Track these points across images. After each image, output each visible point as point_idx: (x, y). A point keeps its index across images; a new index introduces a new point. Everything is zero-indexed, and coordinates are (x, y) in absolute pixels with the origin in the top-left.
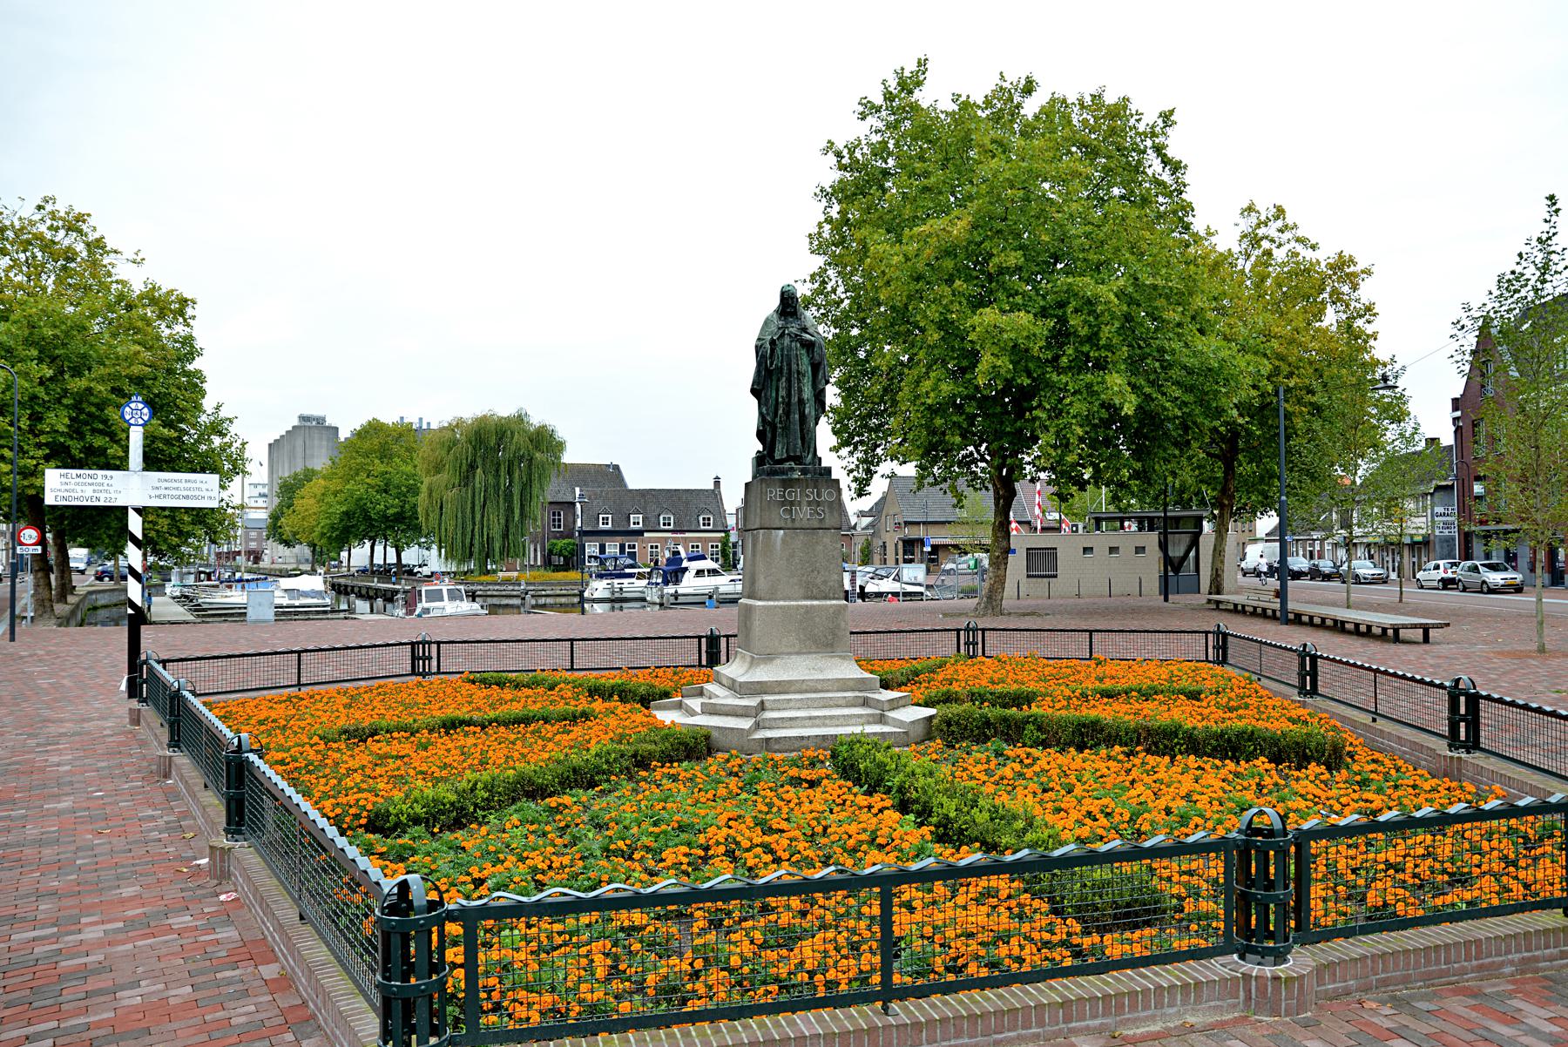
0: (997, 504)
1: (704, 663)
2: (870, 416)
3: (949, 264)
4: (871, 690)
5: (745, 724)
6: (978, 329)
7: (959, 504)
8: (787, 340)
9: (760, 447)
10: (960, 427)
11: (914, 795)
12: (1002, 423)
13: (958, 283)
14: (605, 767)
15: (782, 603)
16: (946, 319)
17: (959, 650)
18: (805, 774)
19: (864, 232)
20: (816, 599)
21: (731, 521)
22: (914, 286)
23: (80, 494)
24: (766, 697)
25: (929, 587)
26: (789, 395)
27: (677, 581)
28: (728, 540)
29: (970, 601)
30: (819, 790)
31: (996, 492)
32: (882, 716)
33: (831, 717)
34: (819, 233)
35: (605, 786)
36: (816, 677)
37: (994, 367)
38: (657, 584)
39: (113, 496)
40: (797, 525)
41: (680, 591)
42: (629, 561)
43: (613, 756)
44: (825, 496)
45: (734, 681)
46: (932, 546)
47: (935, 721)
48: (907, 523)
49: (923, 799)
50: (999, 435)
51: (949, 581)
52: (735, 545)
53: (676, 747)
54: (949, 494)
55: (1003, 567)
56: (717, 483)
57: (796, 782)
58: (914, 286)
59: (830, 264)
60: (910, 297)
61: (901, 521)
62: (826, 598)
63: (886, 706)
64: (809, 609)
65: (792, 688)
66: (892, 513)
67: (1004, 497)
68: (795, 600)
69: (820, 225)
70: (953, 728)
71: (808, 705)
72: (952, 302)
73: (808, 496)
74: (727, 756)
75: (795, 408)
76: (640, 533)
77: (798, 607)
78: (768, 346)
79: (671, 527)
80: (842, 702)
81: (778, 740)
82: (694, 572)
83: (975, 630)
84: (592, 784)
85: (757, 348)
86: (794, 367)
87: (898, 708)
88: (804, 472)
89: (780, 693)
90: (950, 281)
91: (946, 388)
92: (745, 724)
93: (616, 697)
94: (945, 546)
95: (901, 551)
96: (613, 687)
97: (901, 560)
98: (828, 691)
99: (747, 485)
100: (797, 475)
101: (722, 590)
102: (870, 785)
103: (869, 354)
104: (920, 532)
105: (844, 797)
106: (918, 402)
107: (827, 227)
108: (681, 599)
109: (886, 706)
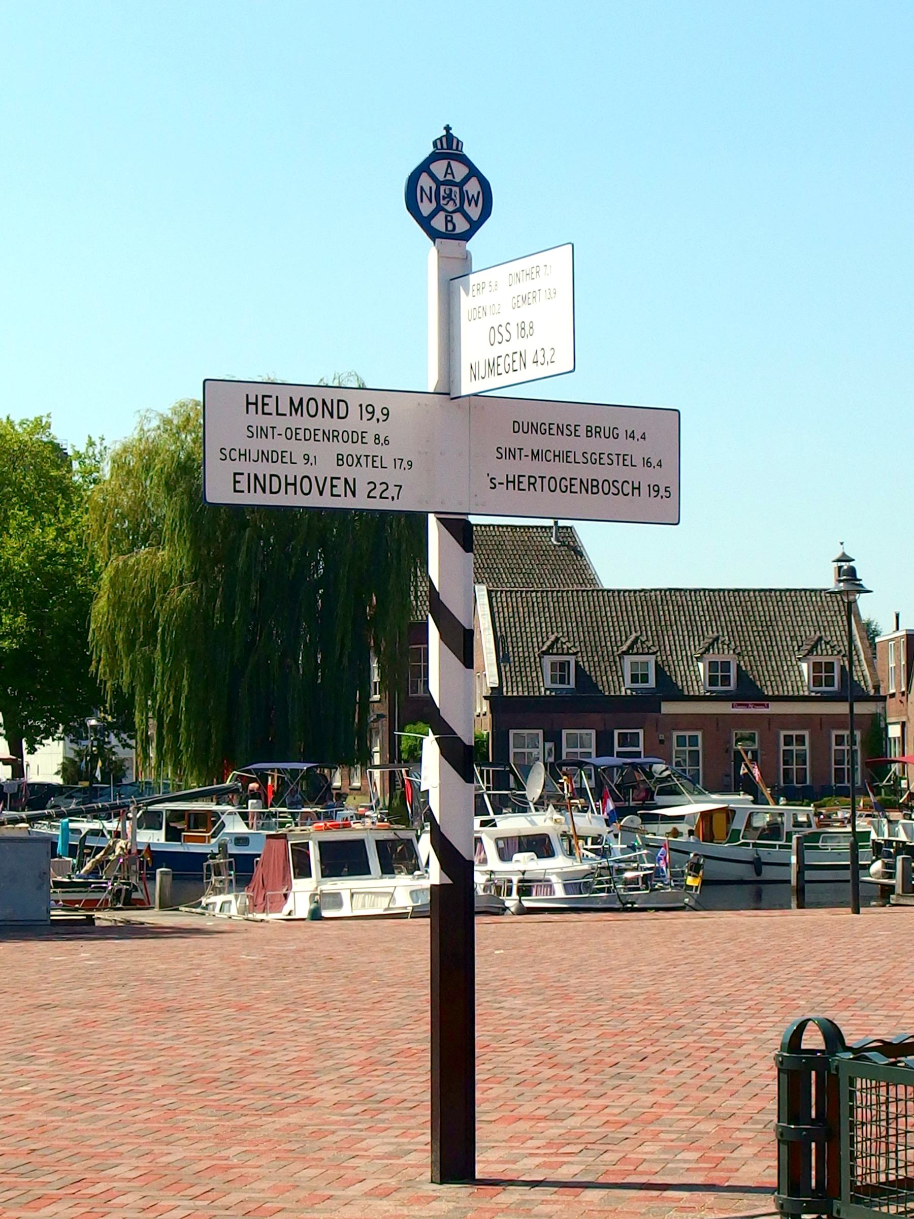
23: (300, 469)
39: (392, 476)
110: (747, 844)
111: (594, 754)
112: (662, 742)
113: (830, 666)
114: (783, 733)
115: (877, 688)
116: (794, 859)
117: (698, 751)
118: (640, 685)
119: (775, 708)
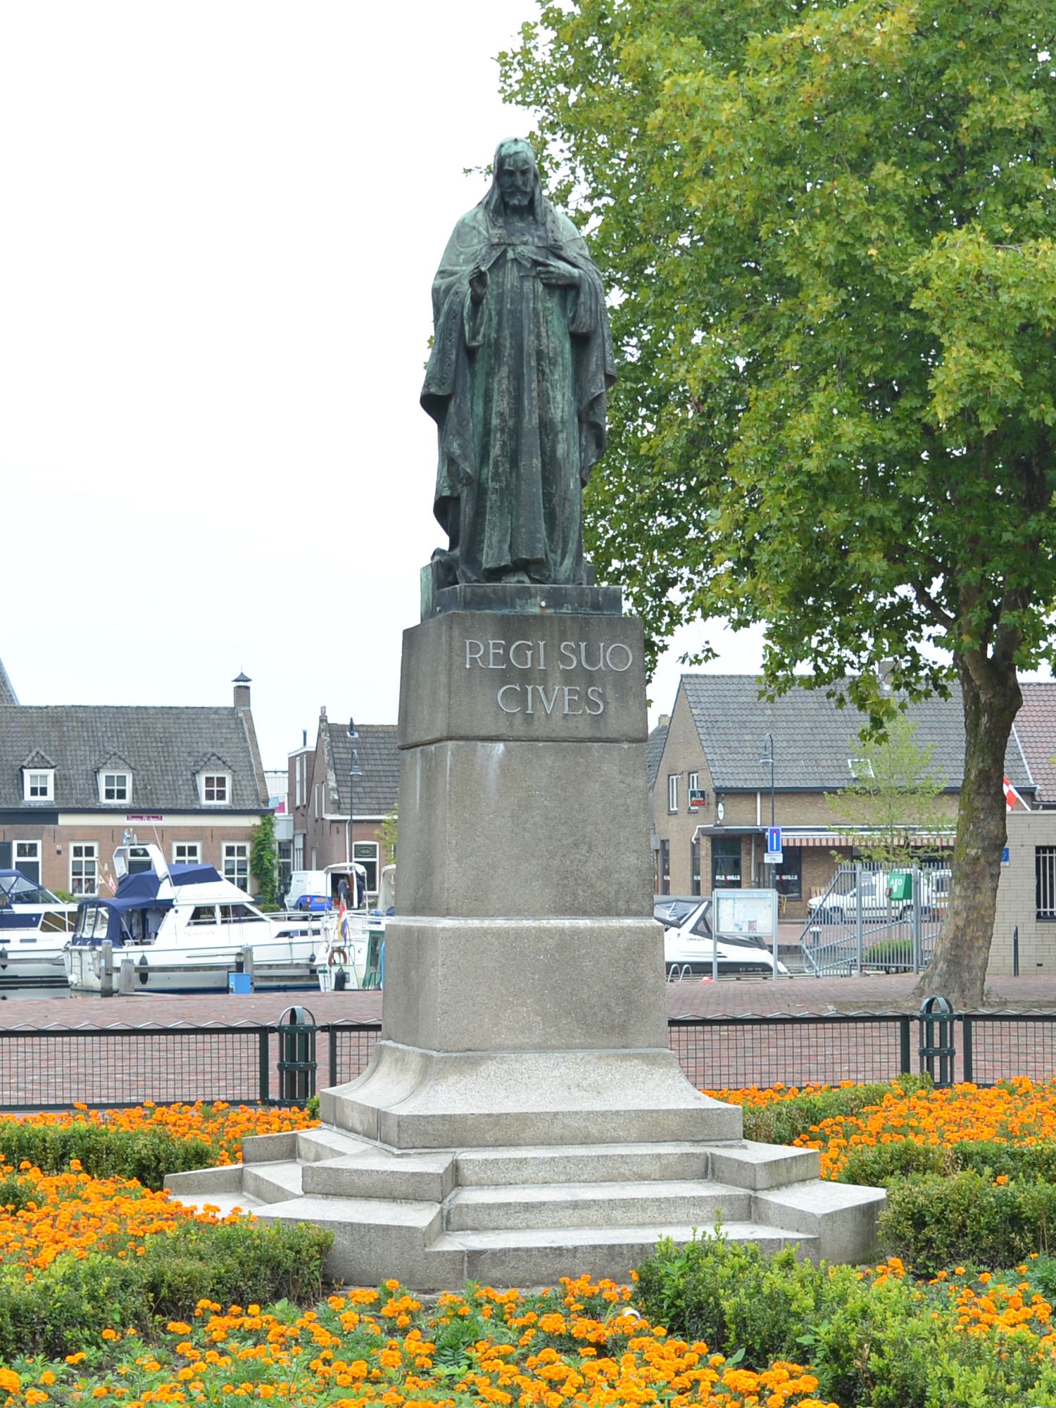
0: (972, 726)
1: (274, 1095)
2: (651, 507)
3: (859, 122)
4: (723, 1138)
5: (420, 1216)
6: (936, 283)
8: (511, 276)
9: (442, 540)
10: (884, 531)
11: (875, 1363)
12: (990, 521)
13: (882, 169)
14: (87, 1307)
15: (500, 923)
16: (853, 260)
17: (906, 1067)
18: (582, 1327)
19: (648, 42)
20: (585, 913)
21: (277, 789)
22: (773, 177)
24: (465, 1155)
25: (786, 952)
26: (517, 410)
27: (146, 935)
28: (268, 835)
29: (894, 979)
30: (629, 1357)
31: (972, 699)
32: (752, 1202)
33: (628, 1204)
34: (526, 52)
35: (86, 1354)
36: (586, 1107)
37: (976, 377)
38: (95, 942)
40: (539, 729)
41: (153, 960)
42: (25, 886)
43: (106, 1281)
45: (380, 1116)
46: (787, 851)
47: (885, 1215)
48: (723, 793)
49: (898, 1369)
50: (981, 550)
51: (830, 935)
52: (285, 849)
53: (251, 1267)
54: (851, 708)
55: (987, 884)
56: (242, 691)
57: (568, 1345)
58: (773, 177)
59: (552, 127)
60: (763, 205)
61: (708, 788)
62: (608, 911)
63: (762, 1179)
64: (566, 940)
65: (529, 1133)
66: (682, 766)
67: (991, 710)
68: (534, 915)
69: (527, 32)
70: (931, 1232)
71: (567, 1173)
72: (867, 217)
73: (565, 660)
74: (374, 1293)
75: (531, 442)
76: (47, 816)
77: (541, 933)
78: (466, 288)
79: (127, 801)
81: (500, 1256)
82: (191, 911)
83: (947, 1020)
84: (56, 1350)
85: (439, 296)
86: (529, 341)
87: (788, 1184)
88: (555, 599)
89: (497, 1144)
90: (861, 167)
91: (852, 431)
92: (420, 1216)
93: (75, 1164)
94: (821, 853)
95: (706, 864)
96: (65, 1141)
97: (706, 885)
98: (615, 1141)
99: (409, 635)
100: (537, 607)
101: (259, 956)
102: (749, 1351)
103: (649, 353)
104: (756, 816)
105: (695, 1374)
106: (781, 469)
107: (546, 35)
108: (155, 980)
109: (762, 1179)
112: (59, 852)
117: (37, 863)
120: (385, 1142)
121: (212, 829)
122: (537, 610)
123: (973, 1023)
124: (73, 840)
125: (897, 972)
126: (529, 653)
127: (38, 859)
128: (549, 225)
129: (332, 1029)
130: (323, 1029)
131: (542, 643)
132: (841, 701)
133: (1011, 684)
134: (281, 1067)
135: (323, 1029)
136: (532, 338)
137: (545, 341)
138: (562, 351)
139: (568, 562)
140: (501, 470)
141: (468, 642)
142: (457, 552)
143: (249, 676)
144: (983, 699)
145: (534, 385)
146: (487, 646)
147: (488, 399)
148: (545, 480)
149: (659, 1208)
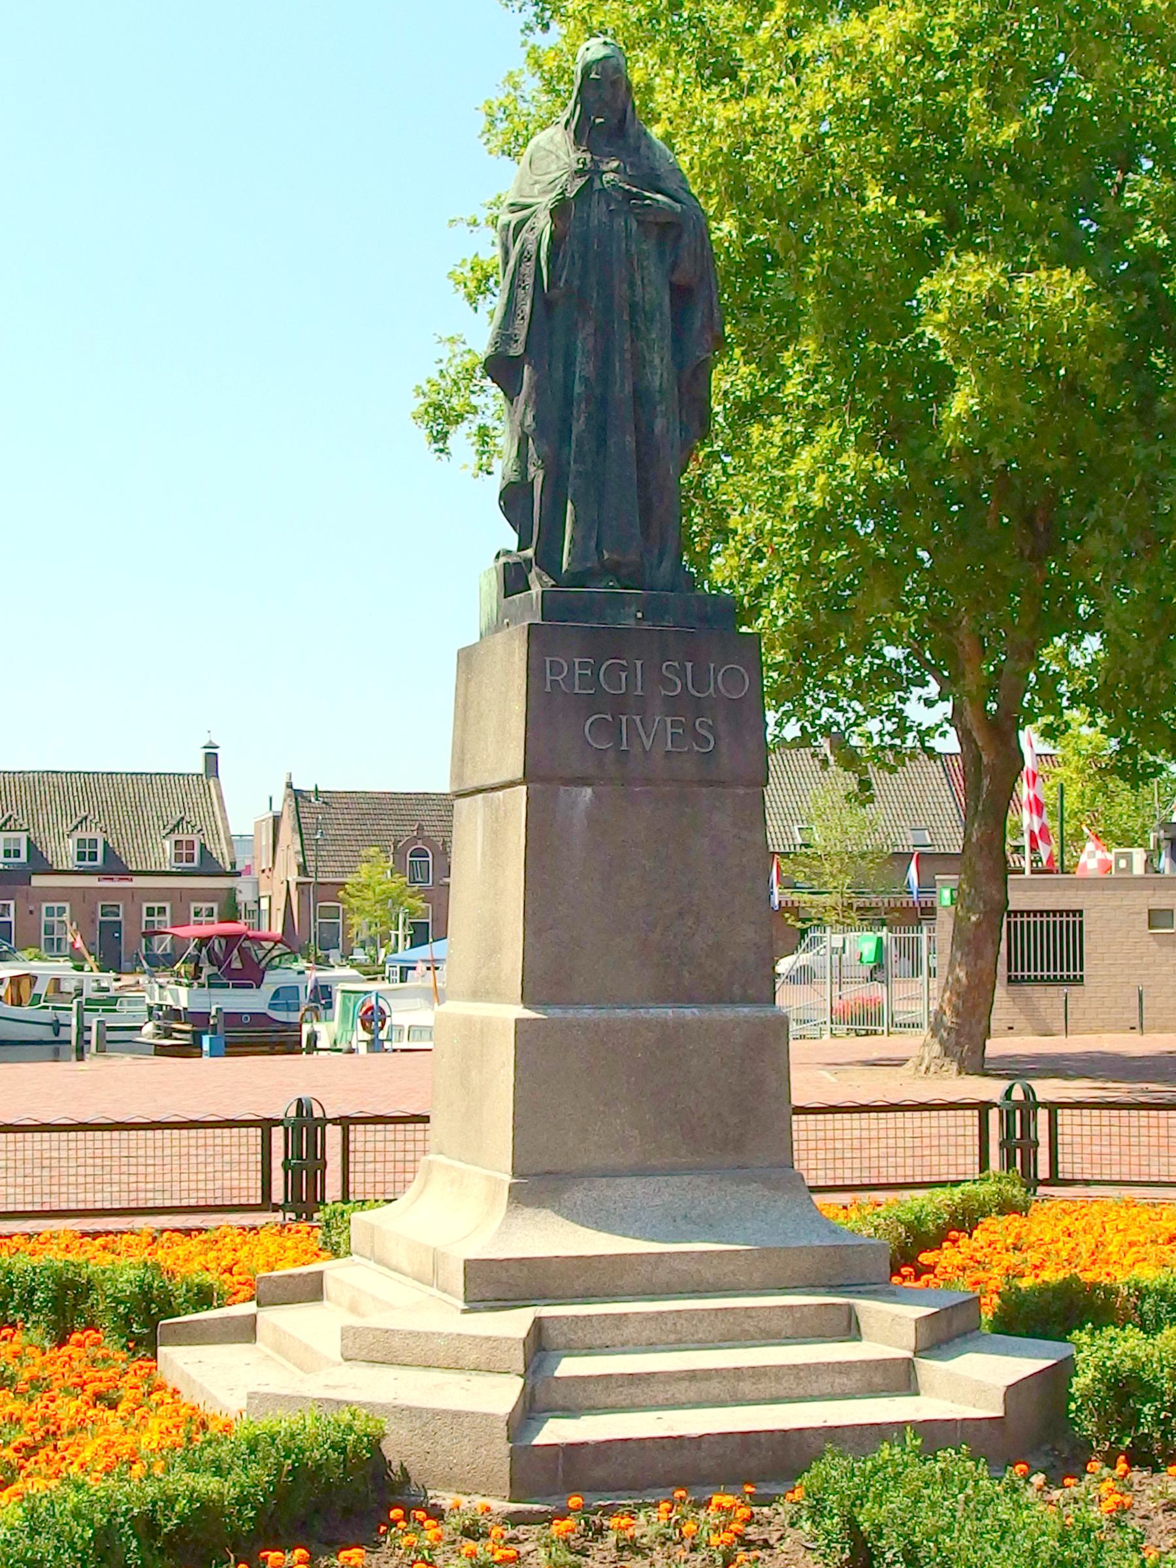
7: (57, 1034)
9: (510, 539)
15: (586, 1013)
17: (984, 1164)
20: (690, 999)
26: (604, 375)
33: (758, 1373)
44: (718, 684)
56: (212, 760)
64: (669, 1035)
73: (667, 683)
80: (785, 1325)
88: (653, 611)
99: (466, 657)
110: (47, 1008)
111: (169, 925)
112: (31, 912)
113: (191, 844)
114: (145, 905)
115: (233, 865)
116: (74, 1022)
117: (10, 923)
118: (12, 860)
119: (139, 882)
120: (445, 1291)
121: (181, 890)
122: (631, 623)
123: (1059, 1111)
124: (45, 901)
125: (867, 1035)
126: (623, 675)
127: (11, 918)
128: (643, 150)
129: (345, 1122)
130: (334, 1121)
131: (639, 663)
132: (825, 762)
133: (1013, 744)
134: (286, 1165)
135: (334, 1121)
136: (625, 286)
137: (639, 290)
138: (660, 305)
139: (667, 565)
140: (586, 448)
141: (548, 659)
142: (530, 553)
143: (217, 744)
144: (985, 759)
145: (627, 346)
146: (571, 667)
147: (569, 365)
148: (639, 461)
149: (797, 1377)
